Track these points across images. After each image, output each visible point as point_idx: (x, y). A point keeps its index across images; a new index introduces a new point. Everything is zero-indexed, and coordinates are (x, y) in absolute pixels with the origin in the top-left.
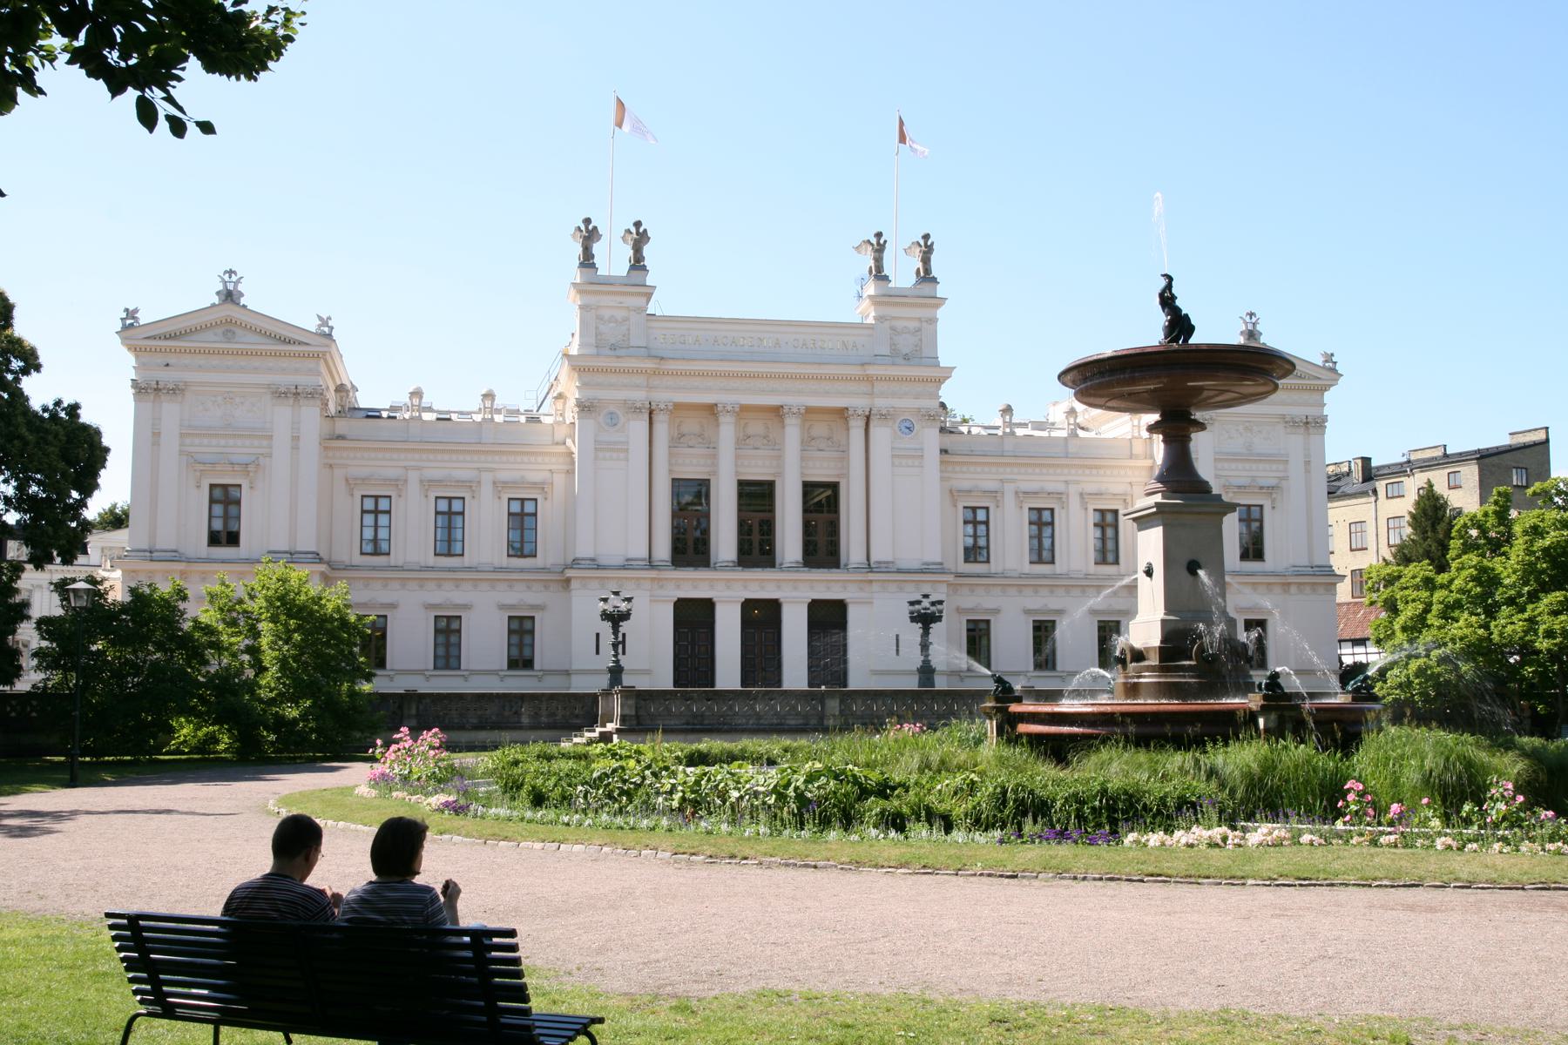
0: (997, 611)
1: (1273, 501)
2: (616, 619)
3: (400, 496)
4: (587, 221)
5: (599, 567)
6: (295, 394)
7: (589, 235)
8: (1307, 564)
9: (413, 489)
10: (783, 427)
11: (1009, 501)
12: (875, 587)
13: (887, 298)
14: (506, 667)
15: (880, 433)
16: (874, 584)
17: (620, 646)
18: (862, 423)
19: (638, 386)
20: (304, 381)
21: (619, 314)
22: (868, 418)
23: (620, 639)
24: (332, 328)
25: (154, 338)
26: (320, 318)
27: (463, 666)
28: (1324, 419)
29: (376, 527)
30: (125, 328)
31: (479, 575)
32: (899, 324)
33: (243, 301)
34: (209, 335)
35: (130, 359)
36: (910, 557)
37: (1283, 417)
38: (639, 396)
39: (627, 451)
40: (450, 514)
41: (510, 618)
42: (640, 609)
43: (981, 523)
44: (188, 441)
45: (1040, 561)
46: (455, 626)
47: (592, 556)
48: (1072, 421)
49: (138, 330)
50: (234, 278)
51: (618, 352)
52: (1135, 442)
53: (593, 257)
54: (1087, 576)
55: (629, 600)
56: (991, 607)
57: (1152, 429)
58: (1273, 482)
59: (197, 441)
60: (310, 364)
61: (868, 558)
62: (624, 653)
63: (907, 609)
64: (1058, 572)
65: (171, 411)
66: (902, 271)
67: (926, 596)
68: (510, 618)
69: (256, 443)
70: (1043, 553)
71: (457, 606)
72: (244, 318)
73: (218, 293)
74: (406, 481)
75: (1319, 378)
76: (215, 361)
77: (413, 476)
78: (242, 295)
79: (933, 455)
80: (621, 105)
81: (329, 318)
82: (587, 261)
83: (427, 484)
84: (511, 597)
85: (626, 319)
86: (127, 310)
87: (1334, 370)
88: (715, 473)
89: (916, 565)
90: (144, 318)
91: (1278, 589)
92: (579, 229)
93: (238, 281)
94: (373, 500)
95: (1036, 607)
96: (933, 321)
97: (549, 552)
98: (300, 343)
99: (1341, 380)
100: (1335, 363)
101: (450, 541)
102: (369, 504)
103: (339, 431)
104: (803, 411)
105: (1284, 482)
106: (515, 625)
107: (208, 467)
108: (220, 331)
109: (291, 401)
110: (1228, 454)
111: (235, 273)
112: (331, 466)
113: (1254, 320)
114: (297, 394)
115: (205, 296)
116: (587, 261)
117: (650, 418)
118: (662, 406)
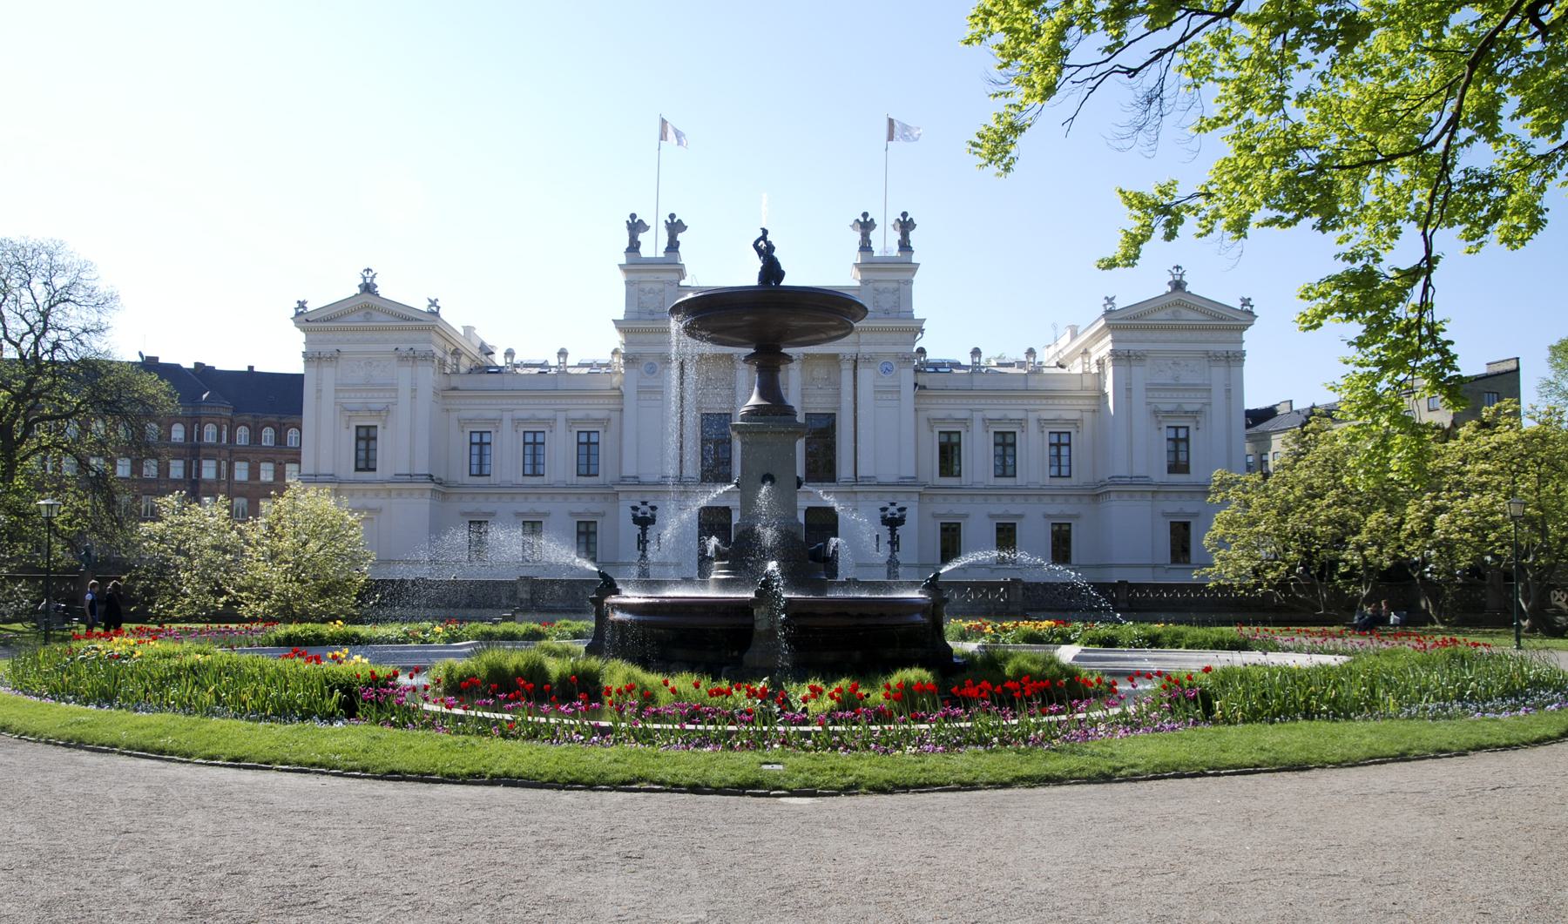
0: (966, 516)
1: (1197, 422)
2: (893, 522)
4: (865, 215)
5: (640, 483)
6: (413, 357)
7: (866, 225)
8: (312, 472)
9: (507, 425)
10: (840, 371)
11: (977, 427)
12: (860, 496)
13: (868, 261)
15: (865, 374)
16: (859, 495)
20: (420, 347)
21: (657, 287)
22: (856, 361)
24: (438, 308)
25: (1121, 319)
26: (430, 300)
28: (1243, 354)
29: (588, 454)
30: (298, 314)
31: (555, 491)
32: (882, 286)
33: (1188, 289)
34: (354, 317)
35: (302, 336)
36: (888, 473)
37: (1207, 352)
40: (588, 443)
41: (579, 523)
42: (911, 516)
43: (363, 439)
44: (341, 395)
45: (1004, 475)
48: (508, 360)
49: (1114, 314)
50: (371, 274)
51: (656, 316)
52: (1084, 376)
53: (870, 242)
56: (489, 511)
57: (748, 359)
58: (1196, 407)
59: (347, 395)
60: (424, 335)
61: (681, 472)
63: (879, 514)
64: (963, 483)
65: (1140, 374)
66: (885, 242)
67: (893, 504)
68: (579, 523)
69: (387, 395)
71: (538, 514)
72: (376, 303)
73: (360, 286)
74: (501, 420)
75: (1237, 320)
76: (358, 336)
77: (507, 416)
79: (908, 390)
80: (664, 122)
81: (437, 300)
82: (634, 247)
83: (571, 422)
84: (579, 507)
85: (662, 291)
86: (1106, 298)
87: (1251, 313)
88: (839, 408)
89: (893, 479)
90: (310, 307)
92: (898, 220)
93: (374, 276)
95: (999, 512)
96: (909, 282)
97: (607, 472)
98: (416, 320)
99: (1257, 321)
100: (1252, 306)
101: (534, 464)
105: (1207, 407)
106: (582, 528)
107: (354, 414)
108: (362, 313)
109: (411, 363)
110: (1158, 384)
112: (448, 410)
113: (1180, 272)
114: (414, 357)
115: (349, 288)
116: (634, 247)
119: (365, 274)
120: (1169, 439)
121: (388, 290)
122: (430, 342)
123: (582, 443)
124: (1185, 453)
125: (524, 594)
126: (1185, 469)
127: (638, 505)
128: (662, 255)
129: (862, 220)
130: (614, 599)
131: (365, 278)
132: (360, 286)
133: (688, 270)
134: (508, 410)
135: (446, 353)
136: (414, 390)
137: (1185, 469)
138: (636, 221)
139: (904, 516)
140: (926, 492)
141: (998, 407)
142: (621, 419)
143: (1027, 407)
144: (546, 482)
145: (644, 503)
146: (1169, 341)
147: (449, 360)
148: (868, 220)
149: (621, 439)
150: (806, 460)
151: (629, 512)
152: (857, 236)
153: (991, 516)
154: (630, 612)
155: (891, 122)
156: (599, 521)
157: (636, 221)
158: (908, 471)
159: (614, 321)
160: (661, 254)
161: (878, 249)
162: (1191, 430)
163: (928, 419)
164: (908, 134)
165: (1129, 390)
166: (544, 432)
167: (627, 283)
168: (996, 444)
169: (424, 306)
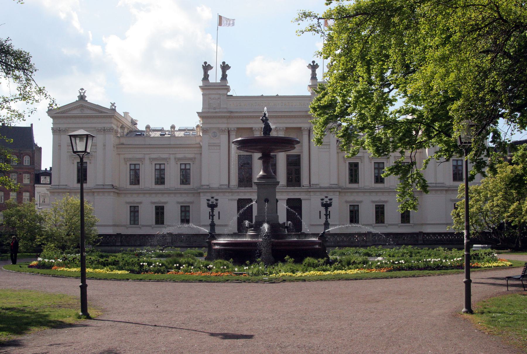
0: (141, 203)
1: (90, 160)
2: (327, 206)
3: (143, 164)
4: (314, 62)
8: (57, 184)
14: (375, 223)
17: (328, 216)
18: (307, 133)
19: (224, 123)
23: (328, 213)
24: (115, 107)
27: (139, 224)
36: (325, 184)
37: (95, 128)
38: (224, 126)
39: (330, 145)
42: (335, 203)
46: (187, 209)
47: (208, 184)
50: (83, 91)
53: (316, 74)
54: (152, 189)
55: (331, 199)
62: (329, 218)
64: (360, 186)
67: (326, 197)
68: (181, 206)
70: (160, 180)
73: (78, 97)
75: (107, 113)
78: (86, 97)
81: (115, 103)
83: (177, 159)
88: (302, 152)
89: (327, 185)
91: (444, 192)
93: (85, 92)
94: (134, 165)
98: (105, 113)
102: (133, 167)
103: (121, 142)
104: (285, 129)
106: (183, 209)
111: (83, 89)
112: (119, 154)
114: (104, 130)
115: (74, 98)
116: (206, 77)
117: (229, 133)
118: (232, 129)
119: (81, 91)
120: (453, 166)
121: (90, 99)
122: (112, 123)
123: (132, 170)
124: (131, 174)
125: (169, 240)
126: (163, 183)
127: (210, 198)
128: (219, 82)
129: (312, 64)
130: (215, 242)
131: (80, 93)
132: (78, 97)
133: (231, 88)
134: (173, 154)
135: (118, 127)
136: (104, 145)
137: (163, 183)
138: (207, 65)
139: (331, 203)
140: (341, 190)
141: (164, 152)
142: (201, 158)
143: (170, 152)
144: (192, 187)
145: (212, 198)
146: (69, 123)
147: (119, 130)
148: (315, 64)
149: (201, 169)
150: (300, 176)
151: (206, 202)
152: (310, 71)
153: (373, 202)
154: (222, 246)
155: (220, 17)
156: (139, 206)
157: (207, 65)
158: (334, 181)
159: (197, 113)
160: (219, 81)
161: (320, 78)
162: (181, 163)
163: (124, 159)
164: (231, 22)
165: (60, 146)
166: (190, 164)
167: (203, 94)
168: (375, 168)
169: (108, 106)
